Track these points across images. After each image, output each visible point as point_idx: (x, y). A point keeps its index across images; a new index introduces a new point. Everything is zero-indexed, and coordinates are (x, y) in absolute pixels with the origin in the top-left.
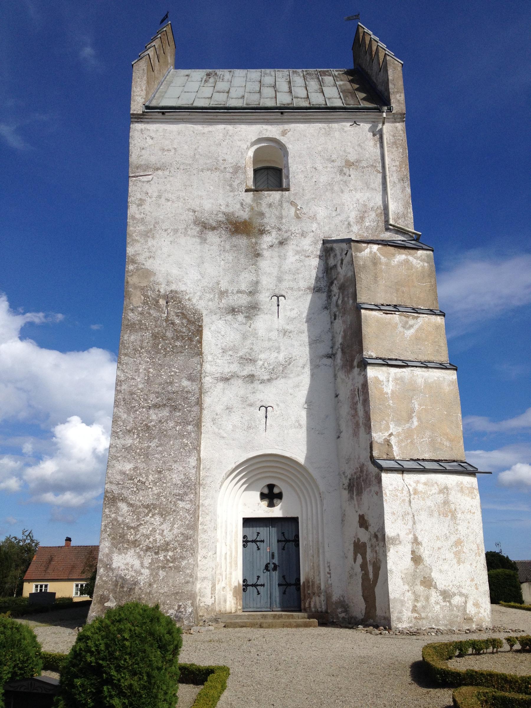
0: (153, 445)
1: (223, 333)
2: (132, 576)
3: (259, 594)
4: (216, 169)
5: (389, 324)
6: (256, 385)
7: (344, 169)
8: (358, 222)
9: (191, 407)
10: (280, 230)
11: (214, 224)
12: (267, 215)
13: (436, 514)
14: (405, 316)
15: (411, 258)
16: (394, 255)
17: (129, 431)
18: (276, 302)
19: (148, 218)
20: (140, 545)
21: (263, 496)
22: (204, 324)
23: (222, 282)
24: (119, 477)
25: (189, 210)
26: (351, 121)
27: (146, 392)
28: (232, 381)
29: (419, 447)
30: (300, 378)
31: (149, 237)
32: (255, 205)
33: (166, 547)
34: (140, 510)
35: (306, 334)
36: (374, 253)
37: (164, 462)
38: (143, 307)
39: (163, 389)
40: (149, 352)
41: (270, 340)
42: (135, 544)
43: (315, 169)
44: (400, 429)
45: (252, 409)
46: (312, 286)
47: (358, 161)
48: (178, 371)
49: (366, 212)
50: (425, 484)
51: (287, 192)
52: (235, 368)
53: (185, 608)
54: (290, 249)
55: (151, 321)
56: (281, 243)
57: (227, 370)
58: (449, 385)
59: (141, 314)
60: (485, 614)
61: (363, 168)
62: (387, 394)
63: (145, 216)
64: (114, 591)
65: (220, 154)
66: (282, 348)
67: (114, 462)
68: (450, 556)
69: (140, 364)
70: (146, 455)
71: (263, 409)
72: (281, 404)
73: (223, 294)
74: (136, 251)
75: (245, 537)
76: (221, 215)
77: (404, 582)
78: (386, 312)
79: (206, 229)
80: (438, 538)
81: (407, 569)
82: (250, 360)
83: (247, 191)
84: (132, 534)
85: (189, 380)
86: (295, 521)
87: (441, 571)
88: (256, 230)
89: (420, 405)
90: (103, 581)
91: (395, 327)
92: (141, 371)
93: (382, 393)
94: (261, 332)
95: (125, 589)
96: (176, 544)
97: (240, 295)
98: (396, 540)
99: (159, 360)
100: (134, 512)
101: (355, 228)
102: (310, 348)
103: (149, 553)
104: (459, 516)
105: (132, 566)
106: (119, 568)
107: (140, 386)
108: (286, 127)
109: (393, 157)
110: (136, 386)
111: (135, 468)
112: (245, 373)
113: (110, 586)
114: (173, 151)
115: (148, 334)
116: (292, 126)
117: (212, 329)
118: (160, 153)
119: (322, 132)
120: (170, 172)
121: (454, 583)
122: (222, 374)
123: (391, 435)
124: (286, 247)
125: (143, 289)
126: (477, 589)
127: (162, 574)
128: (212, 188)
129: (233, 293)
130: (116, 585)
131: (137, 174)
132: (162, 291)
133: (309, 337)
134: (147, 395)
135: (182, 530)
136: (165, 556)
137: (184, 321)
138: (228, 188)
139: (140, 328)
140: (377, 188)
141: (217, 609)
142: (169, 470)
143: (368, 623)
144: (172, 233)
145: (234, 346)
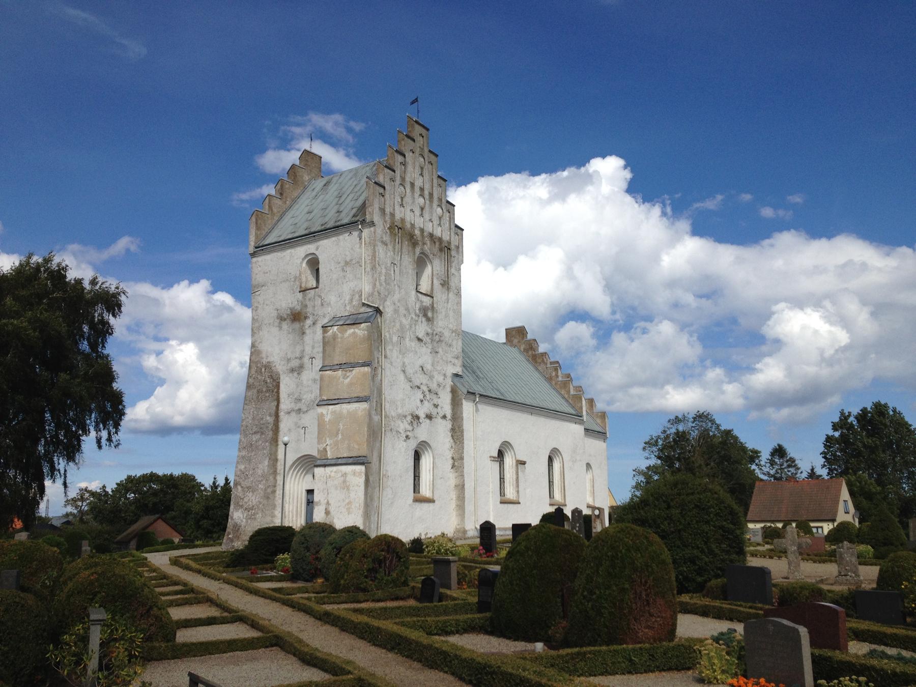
6: (301, 415)
10: (314, 315)
13: (339, 488)
15: (357, 330)
17: (244, 448)
40: (254, 401)
41: (308, 386)
42: (242, 506)
44: (332, 441)
47: (351, 260)
50: (335, 472)
52: (293, 405)
56: (314, 324)
57: (290, 407)
59: (254, 378)
70: (250, 461)
73: (289, 360)
80: (339, 501)
82: (299, 400)
83: (300, 292)
94: (305, 382)
97: (296, 360)
98: (319, 503)
101: (348, 308)
111: (245, 468)
112: (297, 408)
115: (255, 391)
123: (327, 445)
135: (259, 499)
137: (271, 380)
143: (136, 539)
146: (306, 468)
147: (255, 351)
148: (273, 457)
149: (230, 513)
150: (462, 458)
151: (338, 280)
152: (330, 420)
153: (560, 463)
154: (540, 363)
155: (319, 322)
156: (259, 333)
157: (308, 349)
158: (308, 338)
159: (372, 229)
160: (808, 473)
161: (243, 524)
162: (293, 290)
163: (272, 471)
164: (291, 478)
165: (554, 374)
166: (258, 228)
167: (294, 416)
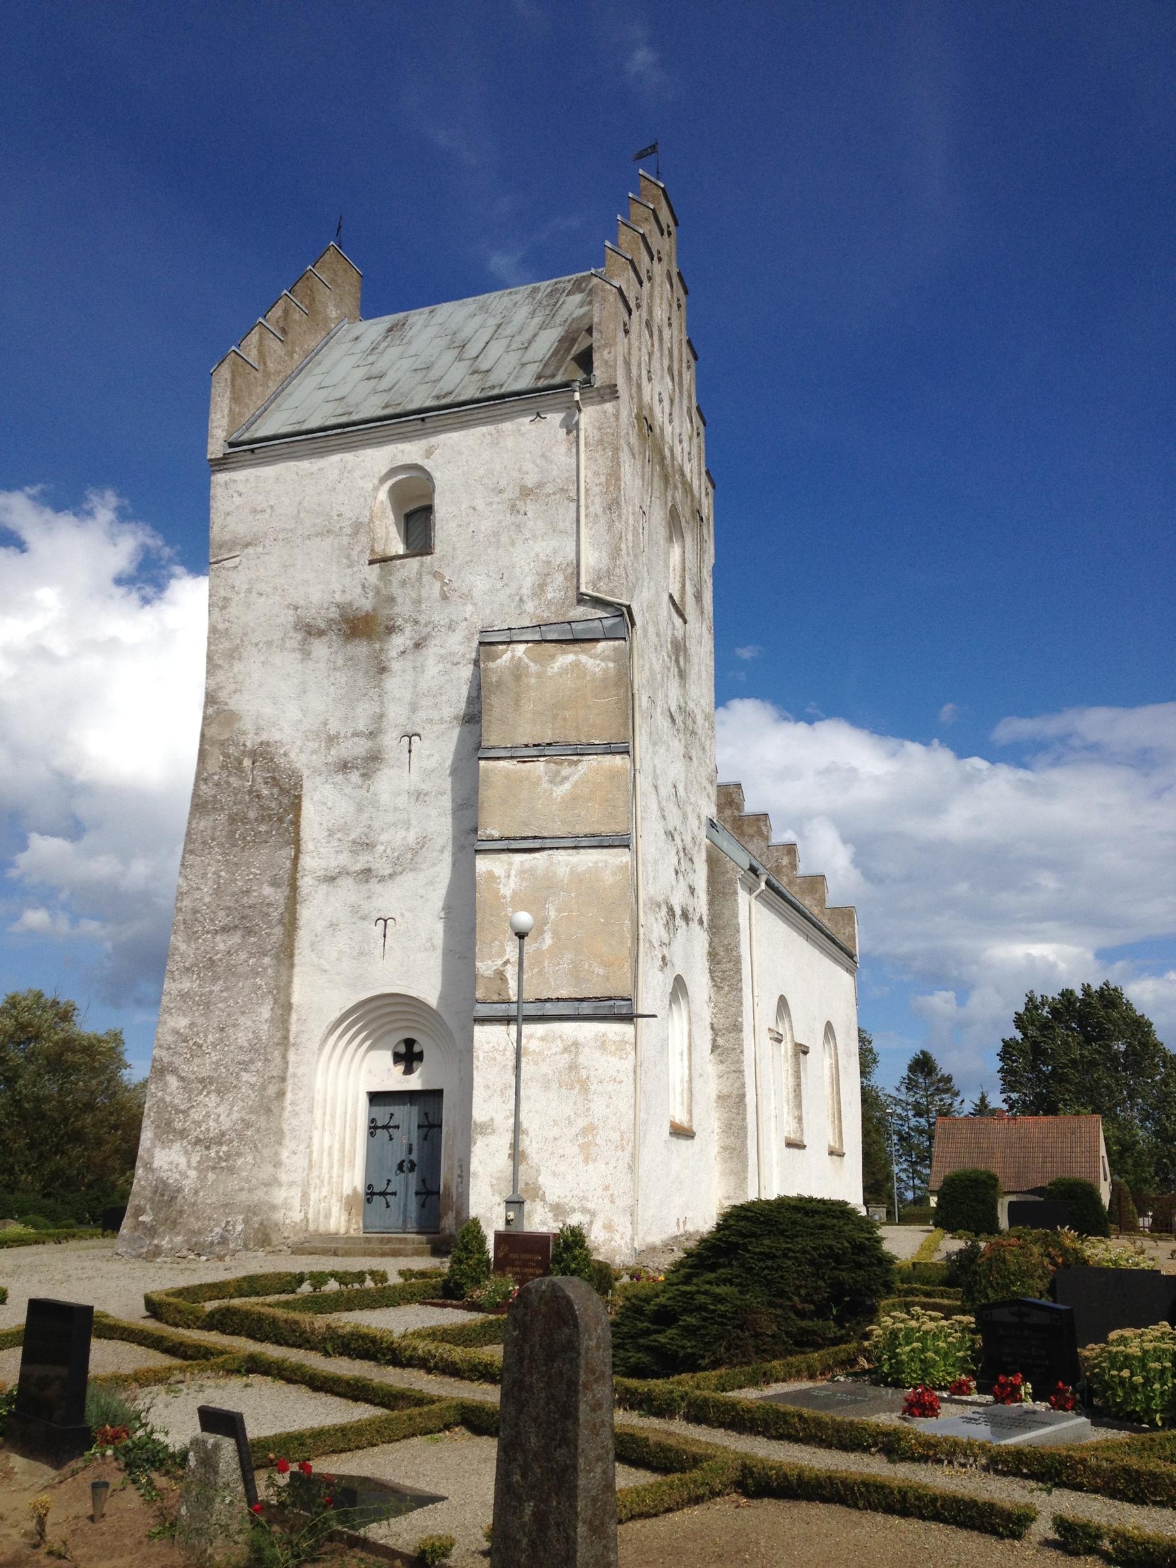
0: (216, 988)
1: (330, 804)
2: (176, 1180)
3: (388, 1206)
4: (328, 532)
5: (527, 778)
6: (374, 885)
7: (518, 502)
8: (534, 594)
9: (271, 927)
10: (416, 622)
11: (323, 626)
12: (399, 600)
13: (555, 1086)
14: (556, 763)
15: (583, 658)
16: (553, 657)
17: (188, 969)
18: (407, 747)
19: (234, 629)
20: (188, 1136)
21: (397, 1058)
22: (303, 792)
23: (332, 720)
24: (170, 1038)
25: (288, 607)
26: (531, 414)
27: (213, 908)
28: (339, 881)
29: (552, 980)
30: (436, 869)
31: (234, 658)
32: (381, 585)
33: (220, 1140)
34: (193, 1085)
35: (449, 793)
36: (519, 658)
37: (229, 1015)
38: (220, 774)
39: (237, 901)
40: (221, 845)
41: (396, 809)
42: (183, 1134)
43: (474, 509)
45: (365, 923)
46: (462, 713)
47: (541, 485)
48: (258, 872)
49: (548, 574)
50: (542, 1039)
51: (429, 557)
52: (344, 859)
53: (234, 1226)
54: (432, 651)
55: (230, 796)
56: (417, 646)
57: (334, 863)
58: (614, 874)
59: (217, 785)
60: (622, 1243)
61: (549, 495)
62: (505, 897)
63: (229, 624)
64: (152, 1201)
65: (334, 505)
66: (414, 822)
67: (166, 1015)
68: (572, 1150)
69: (209, 865)
70: (207, 1005)
71: (381, 922)
72: (407, 914)
73: (332, 740)
74: (218, 683)
75: (373, 1120)
76: (333, 609)
77: (493, 1191)
78: (523, 760)
79: (310, 635)
81: (501, 1171)
82: (365, 845)
83: (371, 562)
84: (180, 1121)
85: (272, 885)
86: (437, 1094)
87: (554, 1174)
88: (382, 629)
89: (559, 910)
90: (141, 1186)
91: (538, 782)
92: (209, 875)
93: (498, 897)
94: (385, 798)
95: (166, 1198)
96: (234, 1135)
97: (356, 739)
98: (487, 1128)
99: (235, 856)
100: (184, 1088)
101: (530, 606)
102: (454, 818)
103: (198, 1148)
104: (593, 1088)
105: (178, 1165)
106: (161, 1167)
107: (207, 899)
108: (433, 440)
109: (596, 469)
110: (201, 899)
111: (192, 1025)
112: (358, 867)
113: (148, 1193)
114: (269, 511)
115: (223, 817)
116: (442, 438)
117: (315, 798)
118: (250, 518)
119: (486, 442)
120: (264, 547)
121: (575, 1193)
122: (326, 870)
123: (506, 963)
124: (424, 651)
125: (222, 745)
126: (613, 1202)
127: (211, 1176)
128: (322, 565)
129: (346, 737)
130: (155, 1192)
131: (220, 558)
132: (249, 744)
133: (453, 800)
134: (214, 913)
135: (243, 1114)
136: (217, 1152)
137: (275, 790)
138: (345, 561)
139: (213, 808)
140: (569, 529)
141: (312, 1227)
142: (234, 1026)
144: (264, 649)
145: (346, 823)
146: (374, 1031)
147: (218, 713)
148: (282, 998)
149: (141, 1151)
150: (737, 1028)
151: (496, 534)
152: (515, 893)
153: (831, 1057)
154: (753, 836)
155: (437, 641)
156: (232, 666)
157: (396, 714)
158: (397, 684)
159: (609, 407)
160: (976, 1105)
161: (188, 1184)
162: (348, 557)
163: (279, 1035)
164: (330, 1057)
165: (785, 861)
166: (236, 399)
167: (347, 890)
